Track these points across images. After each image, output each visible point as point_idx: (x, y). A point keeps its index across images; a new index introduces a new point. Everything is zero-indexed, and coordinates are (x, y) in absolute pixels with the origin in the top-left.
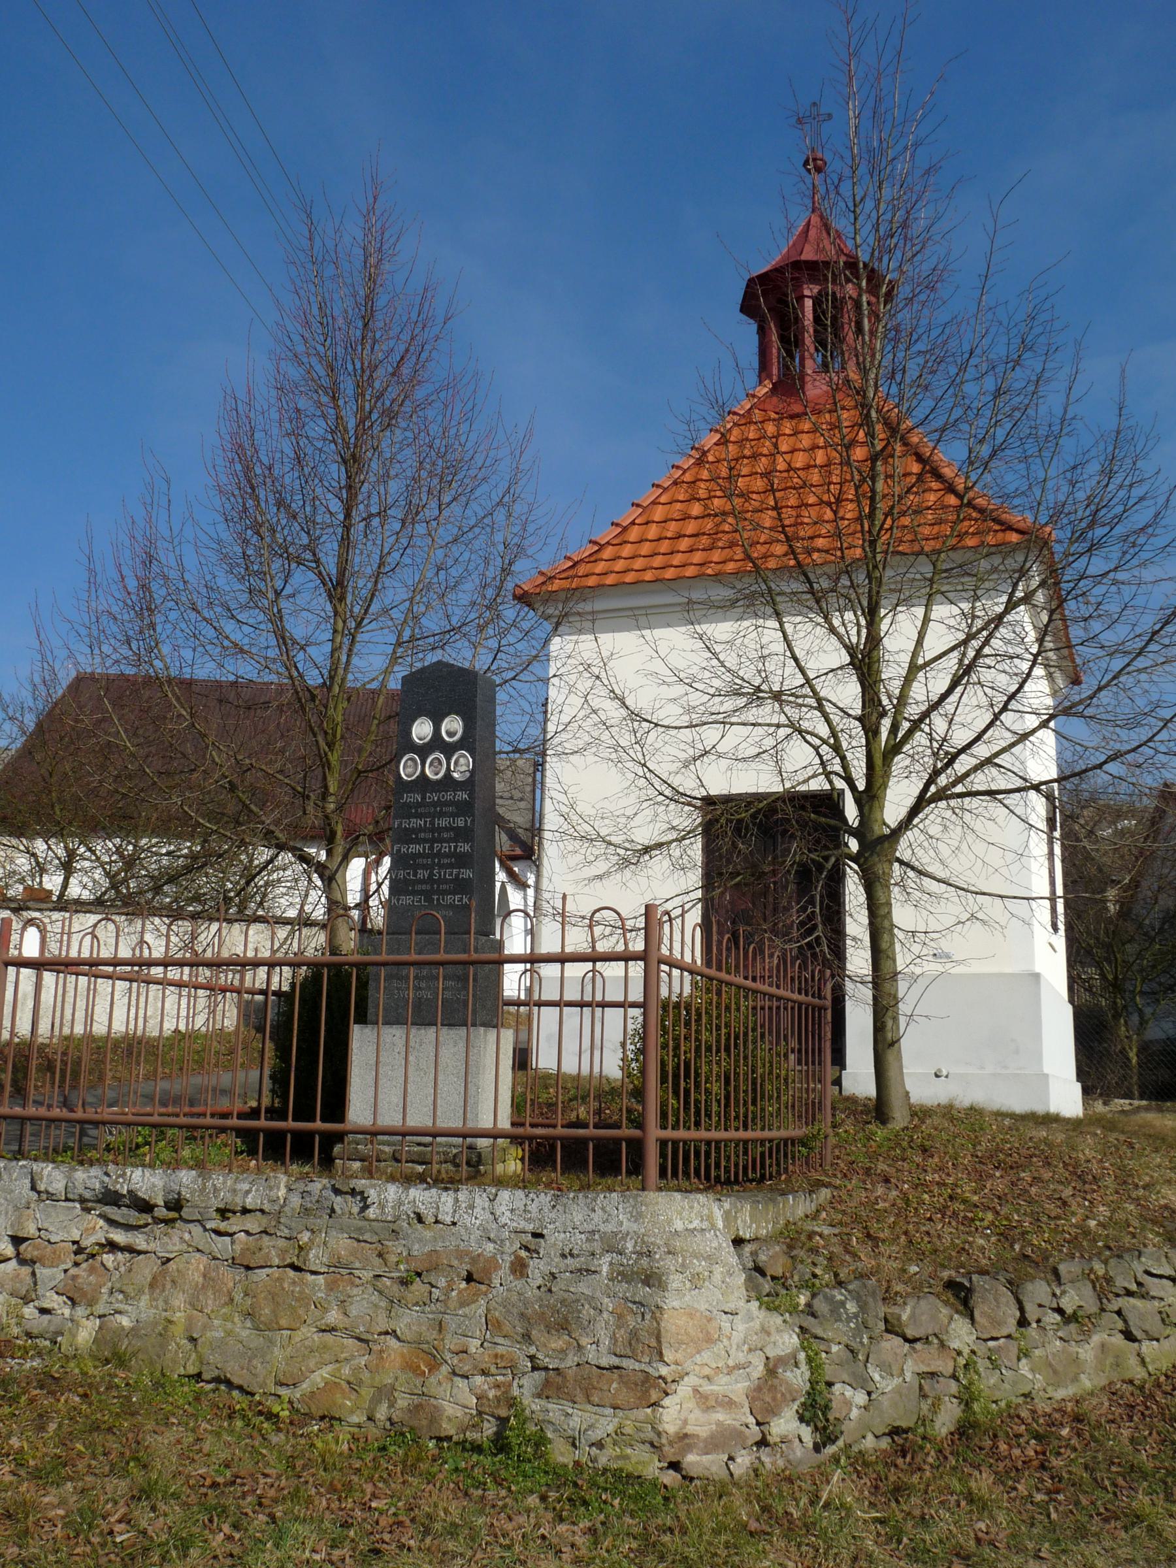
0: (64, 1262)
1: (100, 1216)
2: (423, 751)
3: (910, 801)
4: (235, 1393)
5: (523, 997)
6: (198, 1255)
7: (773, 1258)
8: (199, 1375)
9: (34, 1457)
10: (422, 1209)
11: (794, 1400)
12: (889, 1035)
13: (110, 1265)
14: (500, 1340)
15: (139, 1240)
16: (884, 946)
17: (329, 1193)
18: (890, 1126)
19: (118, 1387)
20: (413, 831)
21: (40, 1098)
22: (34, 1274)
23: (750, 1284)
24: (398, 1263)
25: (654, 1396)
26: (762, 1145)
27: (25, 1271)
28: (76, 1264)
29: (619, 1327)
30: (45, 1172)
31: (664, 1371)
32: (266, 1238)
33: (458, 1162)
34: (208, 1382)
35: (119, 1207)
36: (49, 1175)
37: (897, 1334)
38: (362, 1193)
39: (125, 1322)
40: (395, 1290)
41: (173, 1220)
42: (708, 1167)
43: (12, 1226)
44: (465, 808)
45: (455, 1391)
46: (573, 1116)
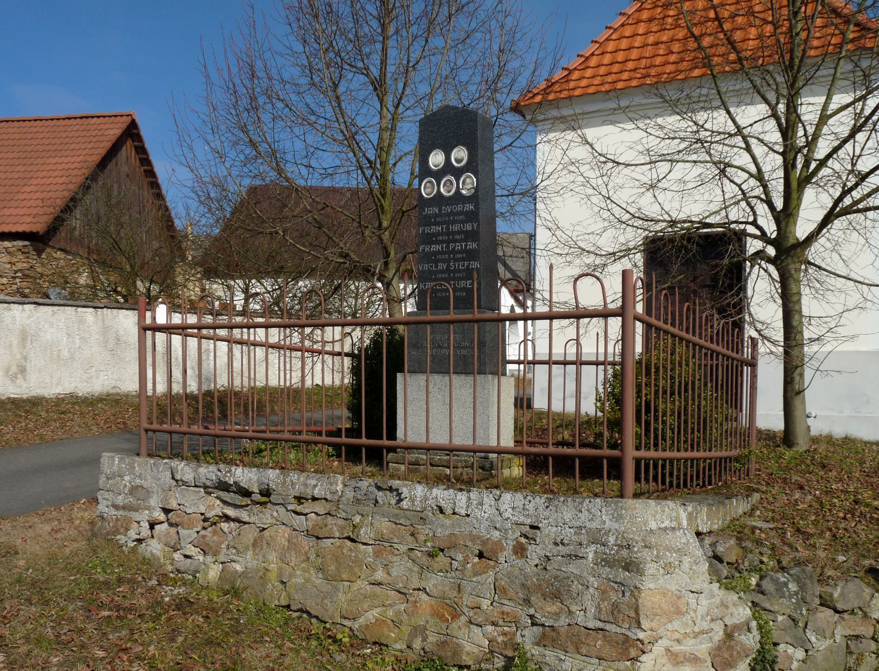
0: (196, 527)
1: (217, 498)
2: (438, 175)
3: (820, 216)
4: (314, 620)
5: (522, 358)
6: (283, 527)
7: (728, 547)
8: (288, 607)
9: (162, 662)
10: (443, 504)
11: (747, 656)
12: (797, 387)
13: (226, 530)
14: (506, 602)
15: (244, 515)
16: (795, 323)
17: (373, 489)
18: (795, 449)
19: (232, 611)
20: (434, 235)
21: (237, 421)
22: (178, 532)
23: (713, 572)
24: (425, 541)
25: (633, 653)
26: (705, 461)
27: (173, 530)
28: (204, 528)
29: (603, 600)
30: (180, 468)
31: (641, 635)
32: (330, 518)
33: (475, 469)
34: (295, 611)
35: (229, 492)
36: (182, 470)
37: (829, 607)
38: (397, 490)
39: (238, 568)
40: (425, 560)
41: (265, 503)
42: (663, 475)
43: (162, 501)
44: (472, 216)
45: (471, 635)
46: (560, 437)
